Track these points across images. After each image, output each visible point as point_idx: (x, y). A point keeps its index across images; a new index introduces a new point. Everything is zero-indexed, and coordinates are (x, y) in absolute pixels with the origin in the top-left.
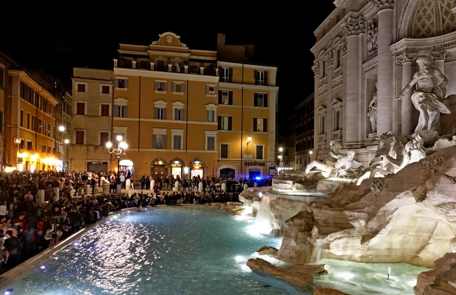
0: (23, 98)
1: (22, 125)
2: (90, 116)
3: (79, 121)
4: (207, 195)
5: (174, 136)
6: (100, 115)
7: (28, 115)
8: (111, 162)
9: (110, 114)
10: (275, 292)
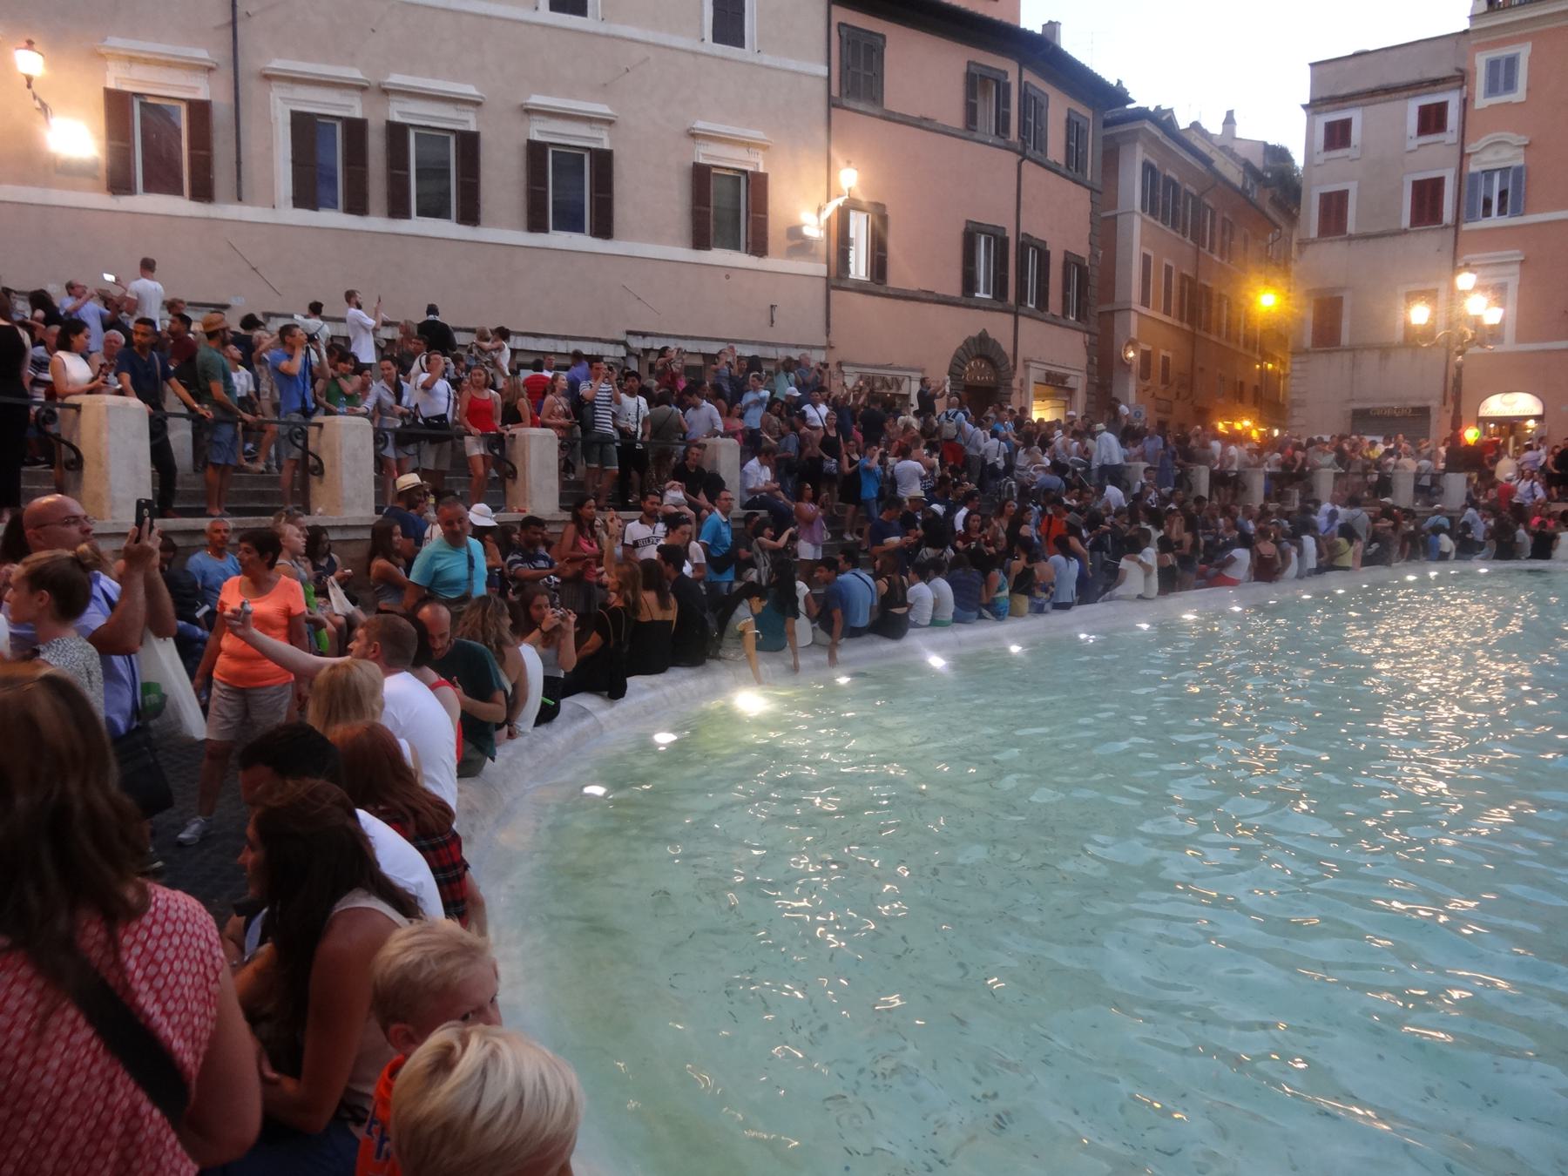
0: (1153, 213)
1: (1145, 301)
2: (1367, 237)
3: (1331, 260)
4: (1240, 420)
5: (1321, 195)
6: (1406, 222)
7: (1168, 269)
8: (1445, 404)
9: (1448, 214)
10: (700, 856)
